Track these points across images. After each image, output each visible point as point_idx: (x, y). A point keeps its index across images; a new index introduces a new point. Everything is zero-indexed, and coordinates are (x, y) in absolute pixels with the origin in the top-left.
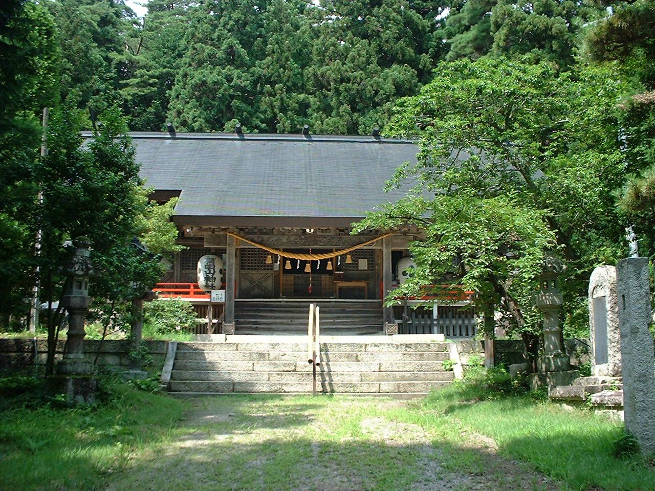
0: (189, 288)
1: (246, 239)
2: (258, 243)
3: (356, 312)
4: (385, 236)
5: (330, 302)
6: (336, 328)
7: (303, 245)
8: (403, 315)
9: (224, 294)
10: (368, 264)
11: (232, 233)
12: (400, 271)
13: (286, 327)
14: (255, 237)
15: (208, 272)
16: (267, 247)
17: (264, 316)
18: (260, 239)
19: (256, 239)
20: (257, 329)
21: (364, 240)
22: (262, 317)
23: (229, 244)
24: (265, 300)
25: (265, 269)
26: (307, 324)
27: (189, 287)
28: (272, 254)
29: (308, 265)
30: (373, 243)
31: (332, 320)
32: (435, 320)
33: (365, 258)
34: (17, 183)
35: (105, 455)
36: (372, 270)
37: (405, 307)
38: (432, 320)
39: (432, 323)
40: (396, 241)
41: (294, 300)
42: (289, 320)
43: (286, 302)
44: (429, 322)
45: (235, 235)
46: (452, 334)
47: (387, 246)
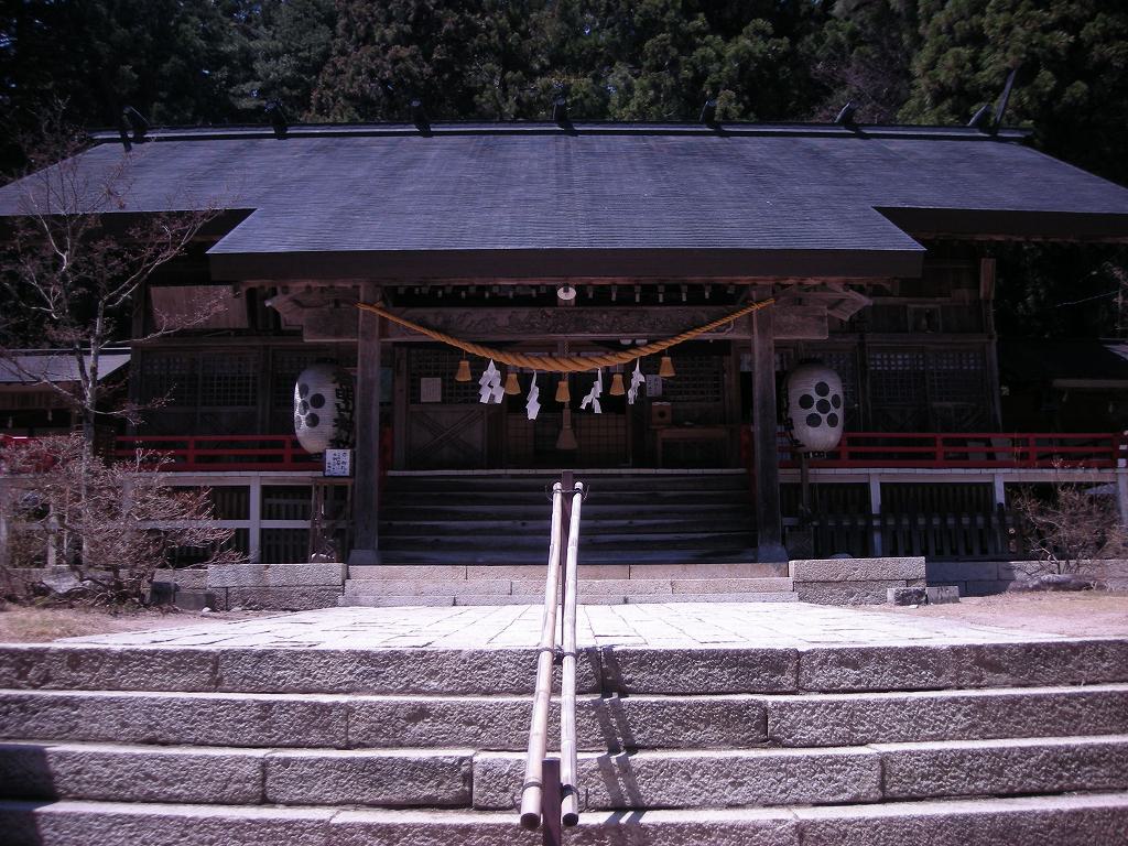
0: (283, 447)
1: (407, 320)
2: (438, 330)
3: (676, 500)
4: (756, 307)
5: (620, 475)
6: (637, 541)
7: (548, 331)
8: (801, 507)
9: (347, 458)
10: (443, 388)
11: (372, 306)
12: (794, 396)
13: (509, 539)
14: (429, 314)
15: (343, 406)
16: (458, 339)
17: (458, 513)
18: (440, 319)
19: (431, 319)
20: (436, 546)
21: (705, 317)
22: (456, 516)
23: (364, 333)
24: (461, 472)
25: (466, 402)
26: (548, 532)
27: (932, 442)
28: (471, 357)
29: (564, 385)
30: (728, 325)
31: (625, 522)
32: (877, 517)
33: (436, 375)
34: (74, 69)
35: (38, 810)
36: (718, 400)
37: (805, 489)
38: (869, 516)
39: (869, 523)
40: (785, 319)
41: (608, 471)
42: (519, 523)
43: (513, 476)
44: (861, 523)
45: (380, 309)
46: (976, 551)
47: (763, 331)
